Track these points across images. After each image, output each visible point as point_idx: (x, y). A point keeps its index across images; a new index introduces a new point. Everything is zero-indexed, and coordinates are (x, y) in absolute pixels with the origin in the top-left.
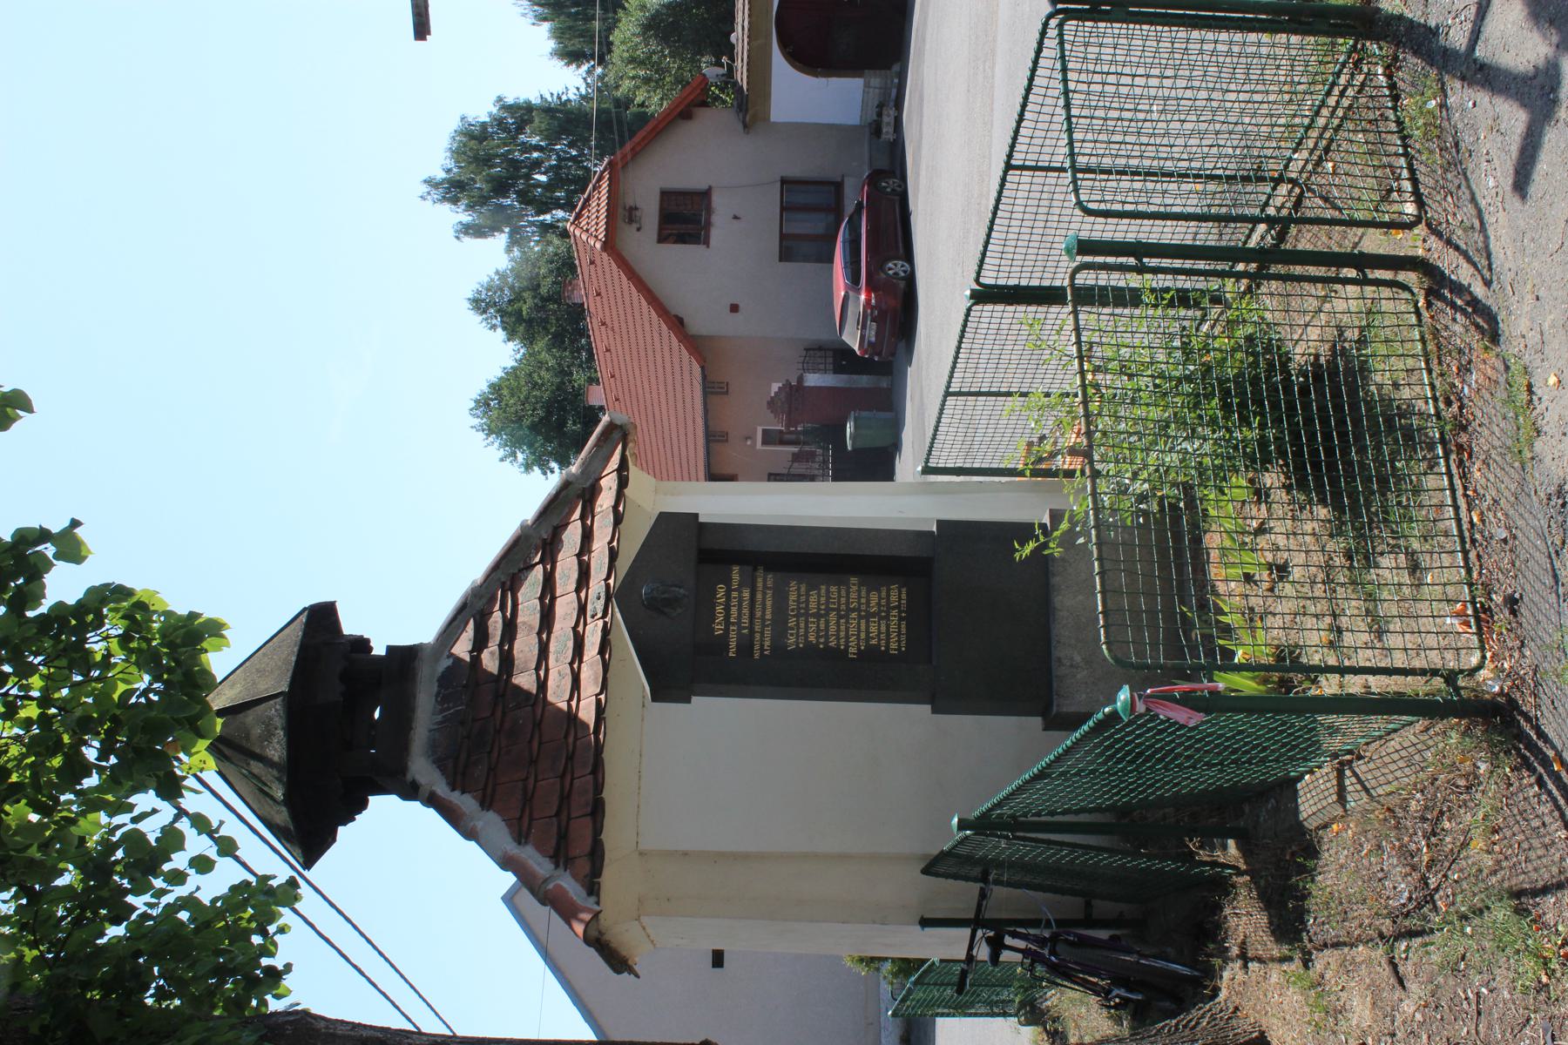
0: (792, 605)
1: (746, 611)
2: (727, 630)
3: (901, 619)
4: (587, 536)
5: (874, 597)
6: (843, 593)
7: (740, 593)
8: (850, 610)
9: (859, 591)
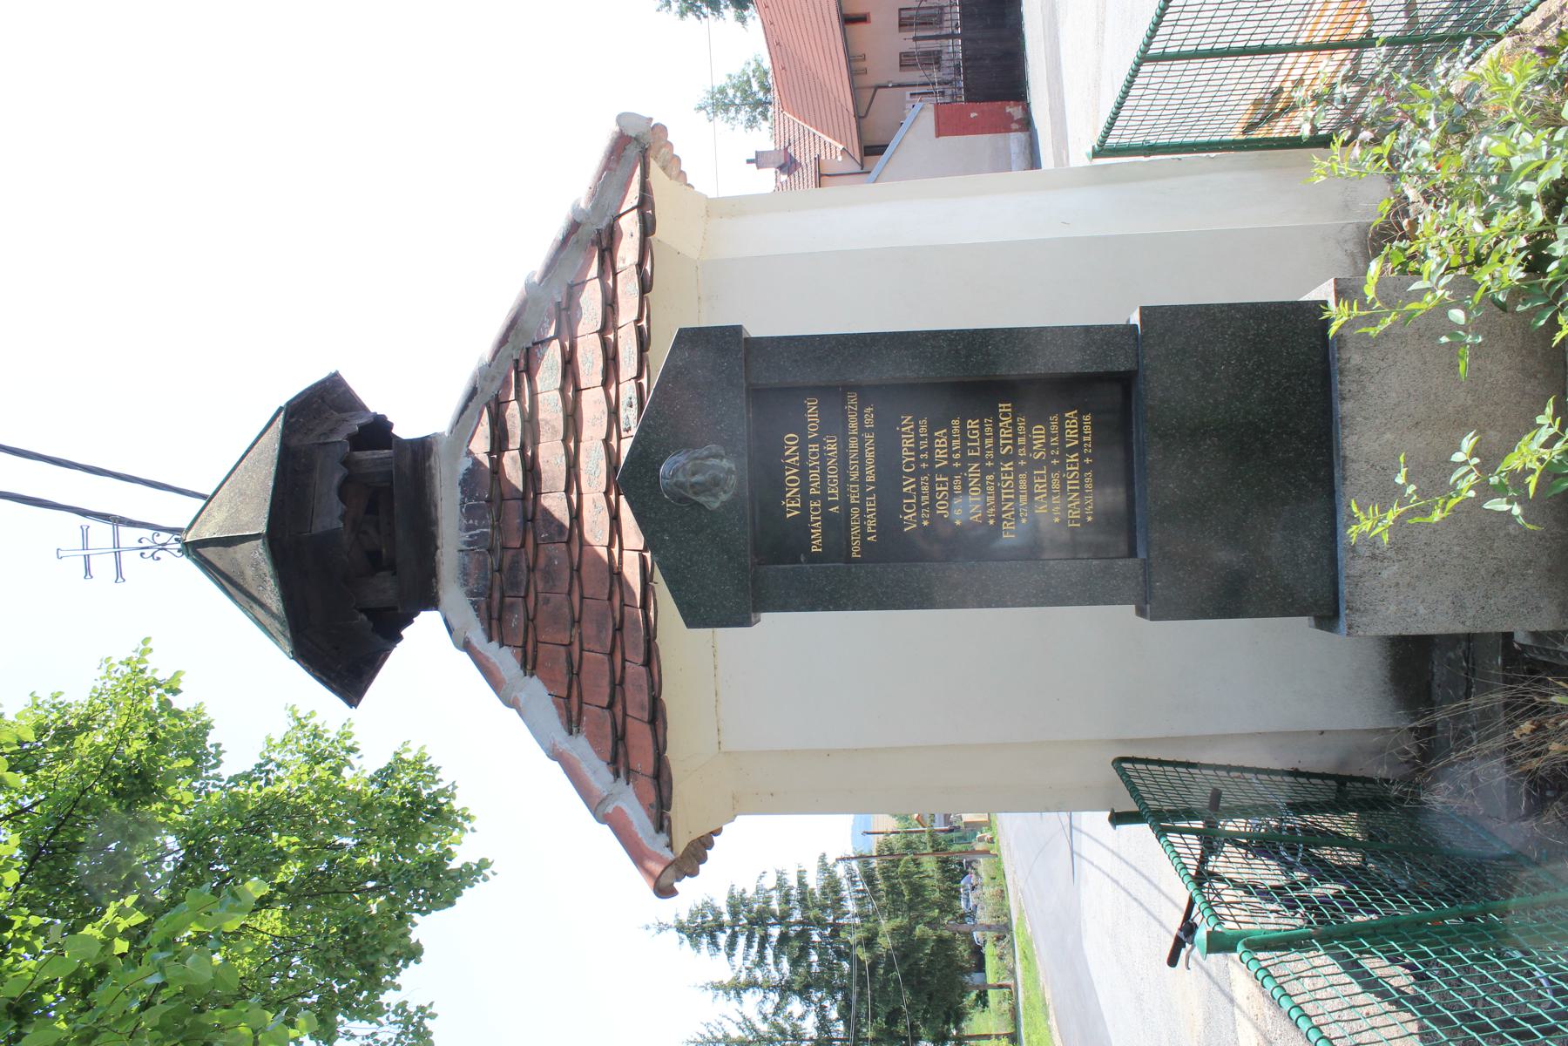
0: (907, 455)
1: (833, 475)
2: (805, 508)
3: (1084, 468)
4: (610, 304)
5: (1039, 432)
6: (989, 430)
8: (999, 459)
9: (1014, 425)
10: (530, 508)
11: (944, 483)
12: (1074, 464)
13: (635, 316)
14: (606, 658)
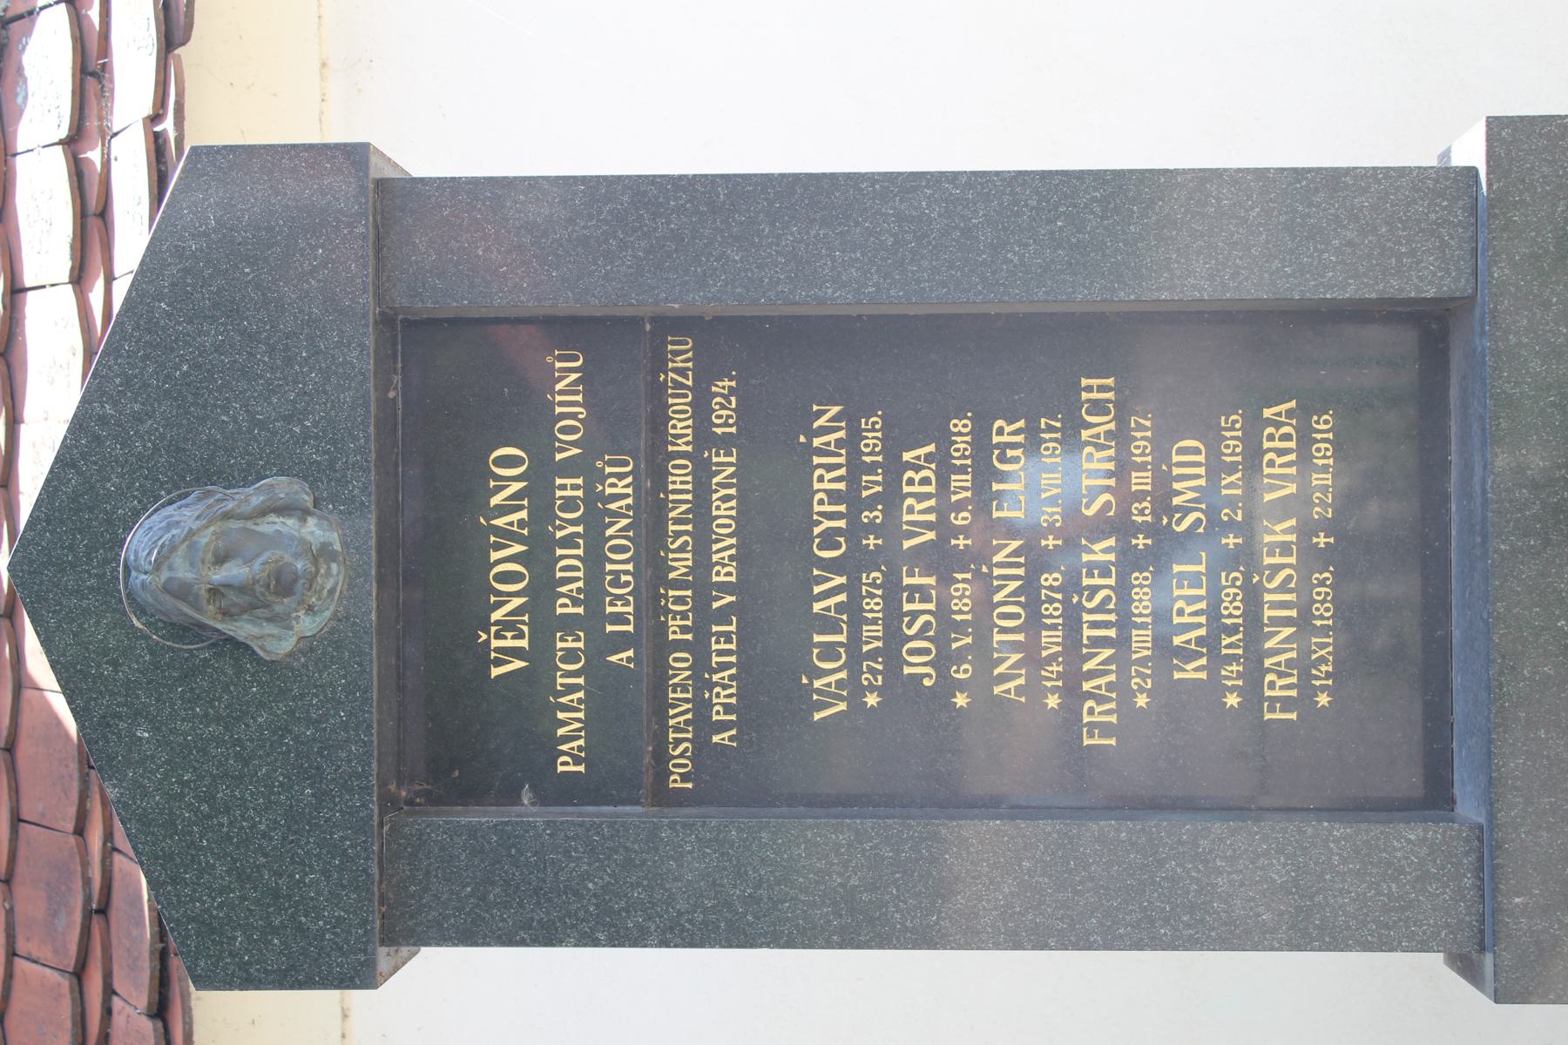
0: (826, 515)
1: (620, 564)
2: (540, 657)
7: (594, 478)
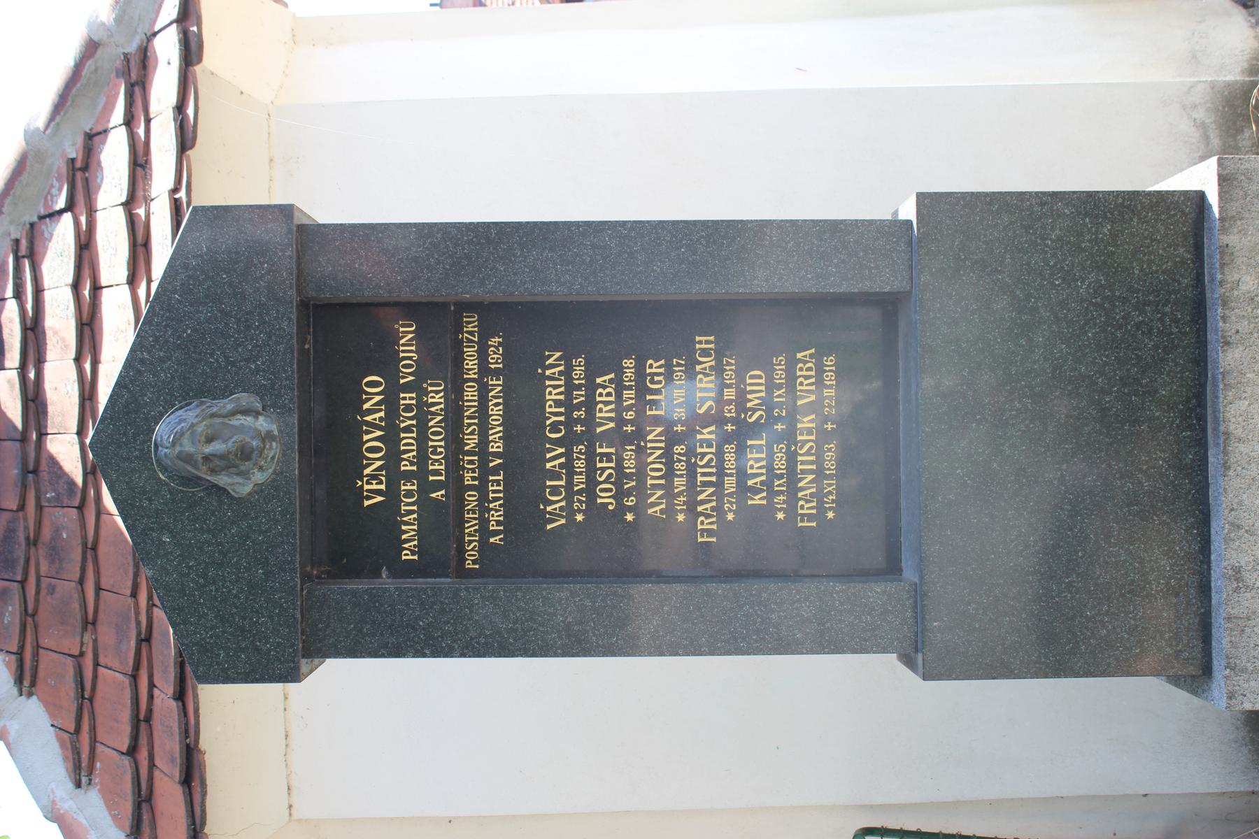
0: (553, 413)
1: (437, 442)
2: (392, 494)
4: (139, 163)
10: (32, 455)
11: (608, 457)
12: (810, 432)
13: (171, 185)
14: (127, 681)
